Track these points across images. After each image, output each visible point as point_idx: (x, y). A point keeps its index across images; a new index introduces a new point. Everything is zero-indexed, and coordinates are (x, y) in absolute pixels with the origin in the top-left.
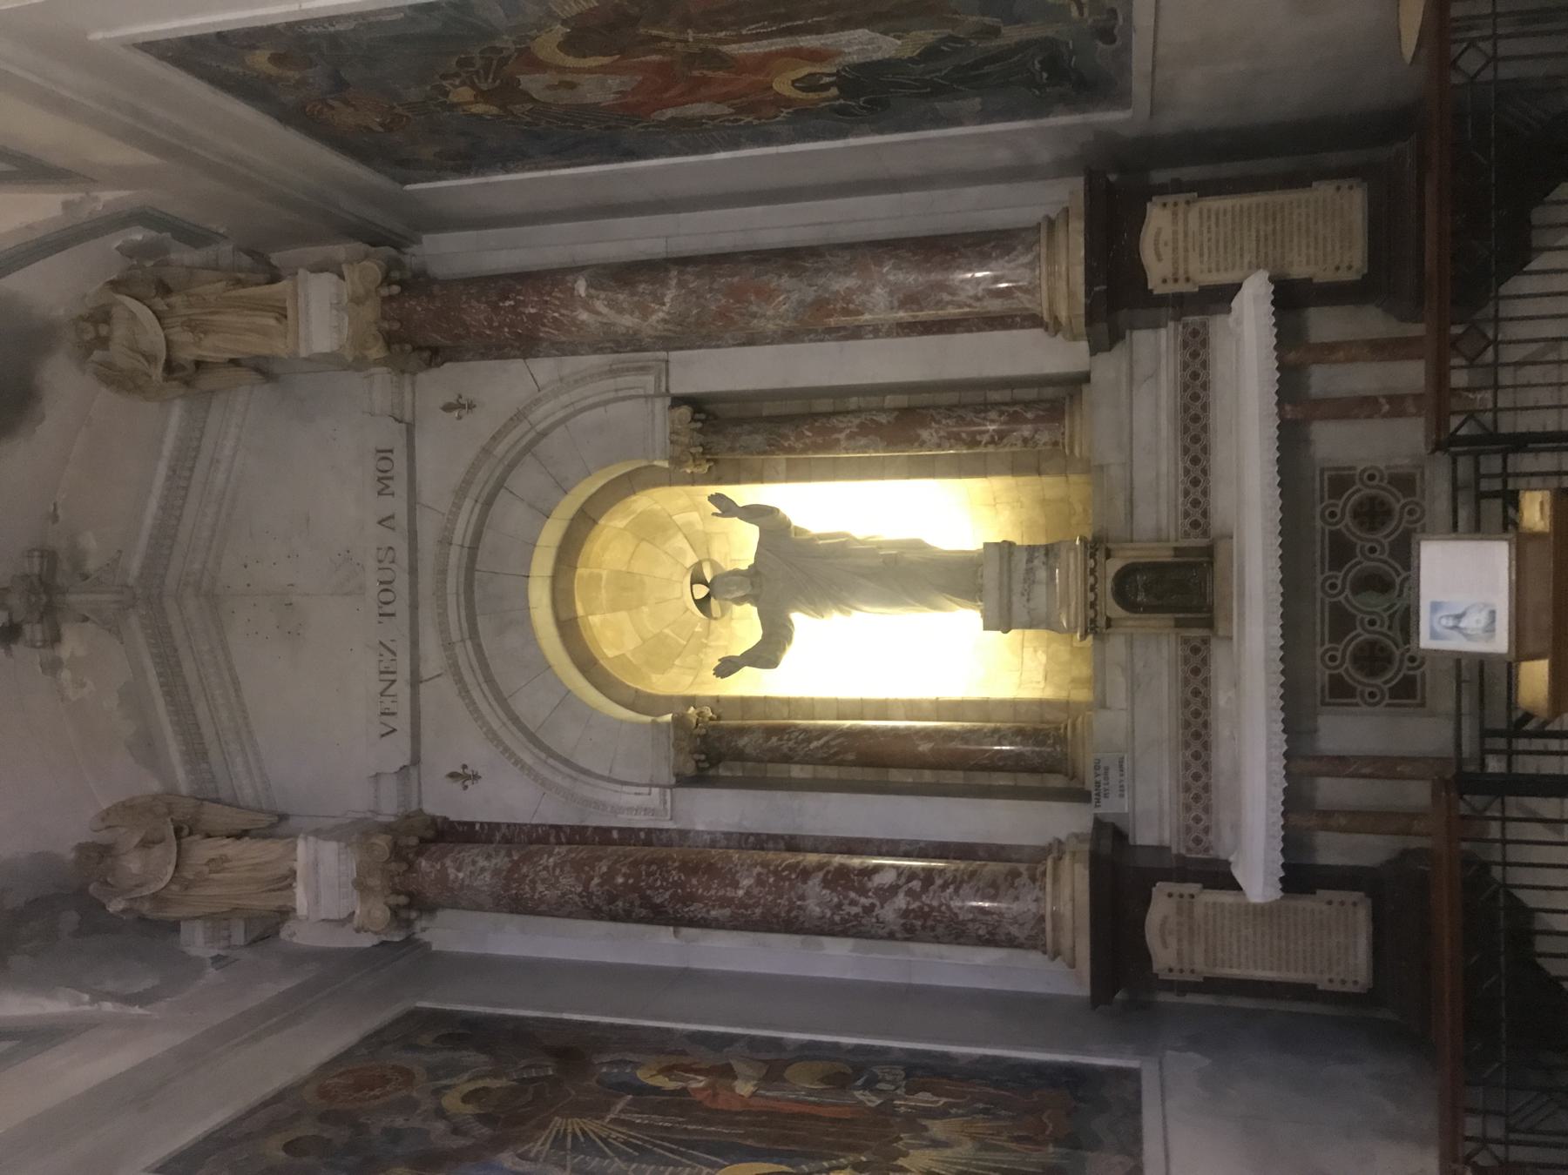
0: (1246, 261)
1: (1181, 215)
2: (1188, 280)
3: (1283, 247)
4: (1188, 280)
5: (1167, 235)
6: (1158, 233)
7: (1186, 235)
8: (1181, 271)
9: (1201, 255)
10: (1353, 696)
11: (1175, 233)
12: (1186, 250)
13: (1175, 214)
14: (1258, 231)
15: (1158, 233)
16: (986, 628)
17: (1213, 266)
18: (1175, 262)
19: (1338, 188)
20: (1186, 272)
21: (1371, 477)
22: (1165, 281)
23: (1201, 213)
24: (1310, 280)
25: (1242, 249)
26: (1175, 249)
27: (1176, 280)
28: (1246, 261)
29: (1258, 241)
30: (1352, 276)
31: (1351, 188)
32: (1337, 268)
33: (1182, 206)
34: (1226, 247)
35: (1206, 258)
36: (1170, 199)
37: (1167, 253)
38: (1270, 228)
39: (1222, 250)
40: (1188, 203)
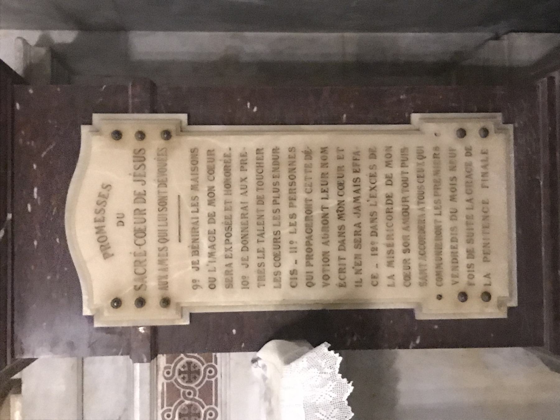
0: (285, 269)
1: (151, 164)
2: (166, 302)
3: (358, 244)
4: (166, 302)
5: (121, 201)
6: (102, 200)
7: (163, 203)
8: (152, 284)
9: (195, 251)
10: (211, 383)
11: (140, 197)
12: (163, 238)
13: (139, 157)
14: (309, 210)
15: (102, 200)
16: (288, 362)
17: (220, 276)
18: (139, 262)
19: (462, 133)
20: (164, 286)
21: (168, 373)
22: (117, 303)
23: (194, 161)
24: (410, 313)
25: (277, 241)
26: (140, 233)
27: (141, 302)
28: (285, 269)
29: (309, 230)
30: (492, 312)
31: (485, 133)
32: (464, 296)
33: (155, 142)
34: (244, 238)
35: (204, 260)
36: (129, 122)
37: (122, 239)
38: (332, 203)
39: (237, 245)
40: (167, 135)
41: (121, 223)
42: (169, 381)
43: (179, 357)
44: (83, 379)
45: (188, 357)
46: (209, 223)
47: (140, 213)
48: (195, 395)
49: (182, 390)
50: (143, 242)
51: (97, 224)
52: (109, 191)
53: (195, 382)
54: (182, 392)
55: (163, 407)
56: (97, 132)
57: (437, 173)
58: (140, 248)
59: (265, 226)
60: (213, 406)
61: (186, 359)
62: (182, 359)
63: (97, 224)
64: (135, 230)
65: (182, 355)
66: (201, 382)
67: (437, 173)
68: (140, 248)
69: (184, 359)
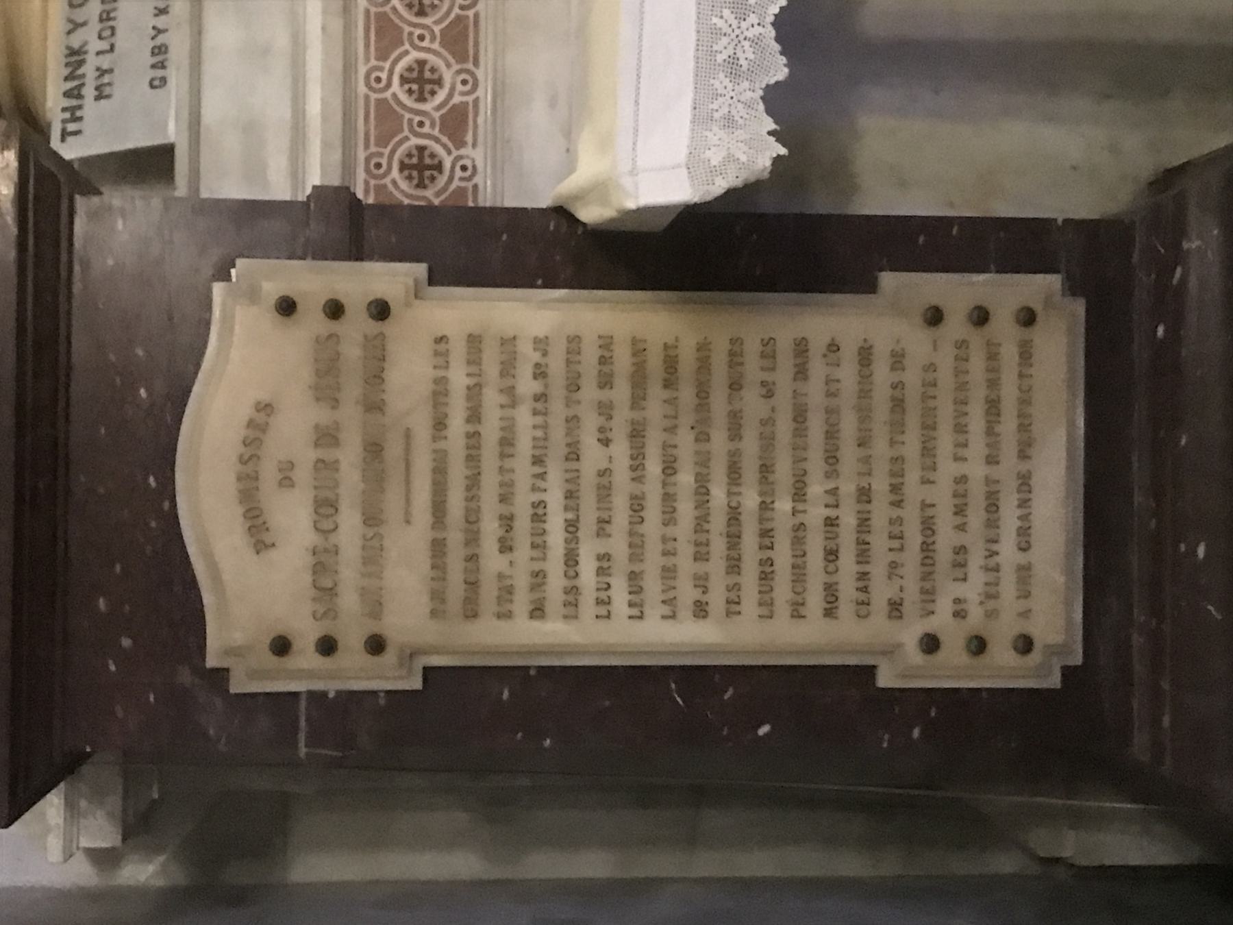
4: (376, 645)
11: (326, 437)
26: (325, 507)
37: (293, 516)
41: (287, 482)
42: (465, 66)
43: (443, 197)
44: (408, 501)
45: (424, 198)
46: (890, 617)
47: (325, 467)
48: (410, 121)
49: (436, 132)
50: (332, 527)
51: (957, 501)
52: (269, 415)
53: (410, 147)
54: (437, 129)
55: (476, 15)
56: (253, 295)
57: (993, 384)
58: (326, 539)
59: (580, 513)
60: (373, 10)
61: (429, 193)
62: (438, 194)
63: (957, 501)
64: (316, 501)
65: (436, 202)
66: (401, 17)
67: (993, 384)
68: (326, 539)
69: (431, 195)
